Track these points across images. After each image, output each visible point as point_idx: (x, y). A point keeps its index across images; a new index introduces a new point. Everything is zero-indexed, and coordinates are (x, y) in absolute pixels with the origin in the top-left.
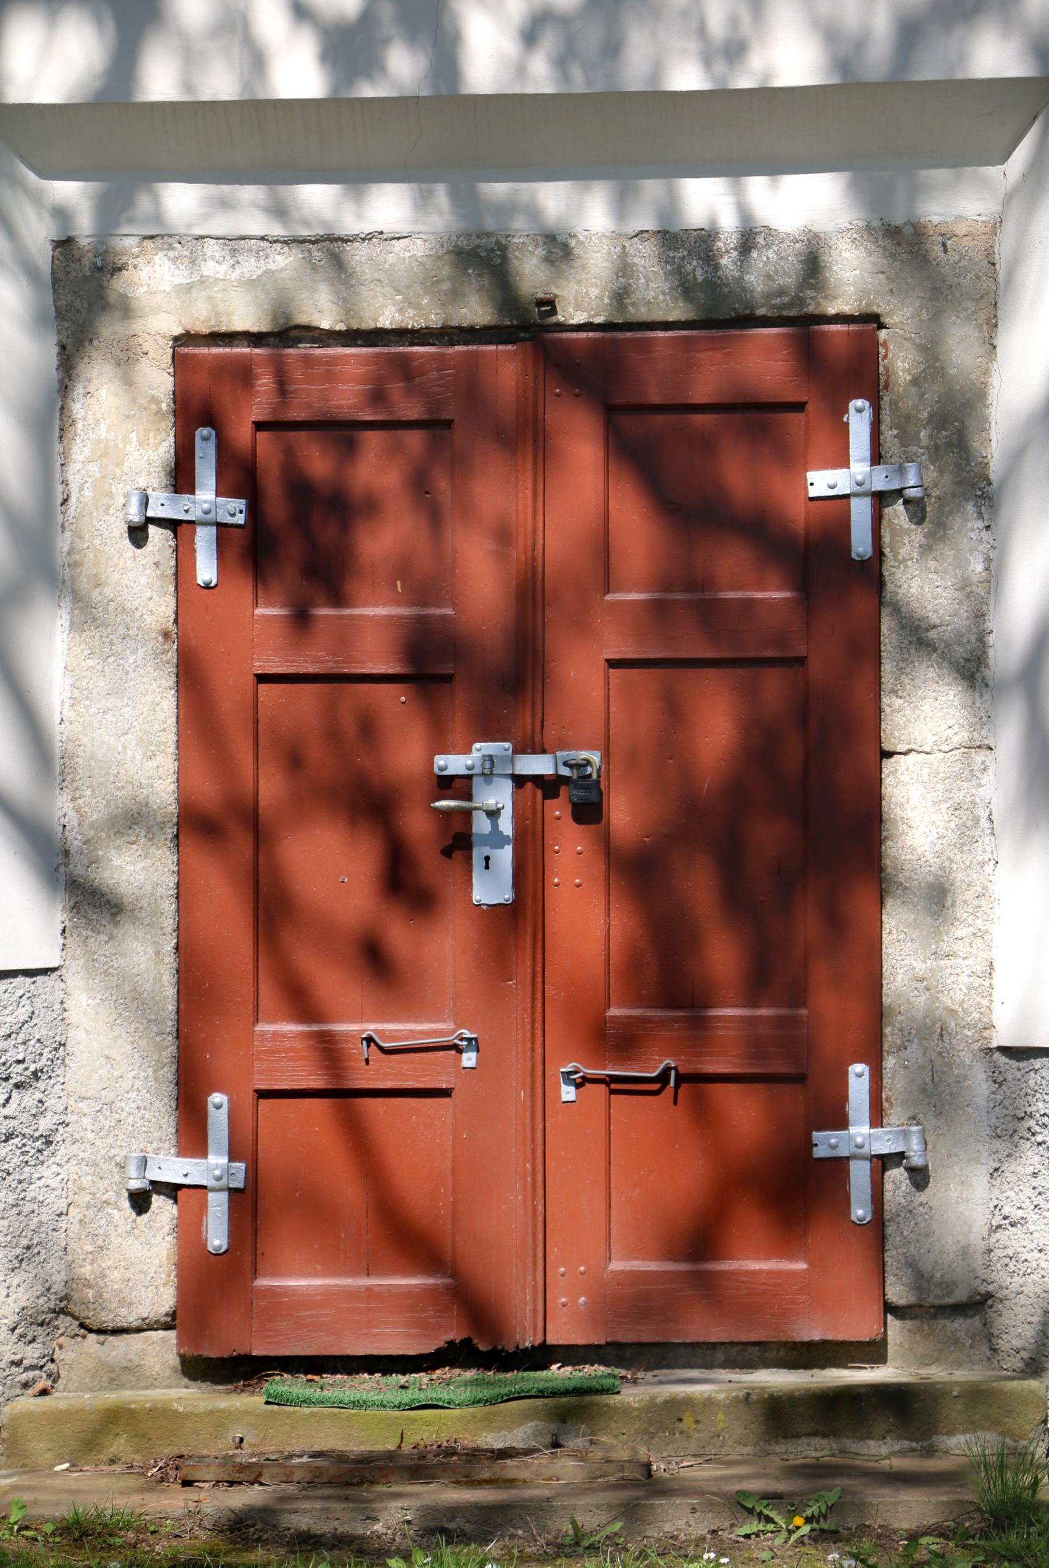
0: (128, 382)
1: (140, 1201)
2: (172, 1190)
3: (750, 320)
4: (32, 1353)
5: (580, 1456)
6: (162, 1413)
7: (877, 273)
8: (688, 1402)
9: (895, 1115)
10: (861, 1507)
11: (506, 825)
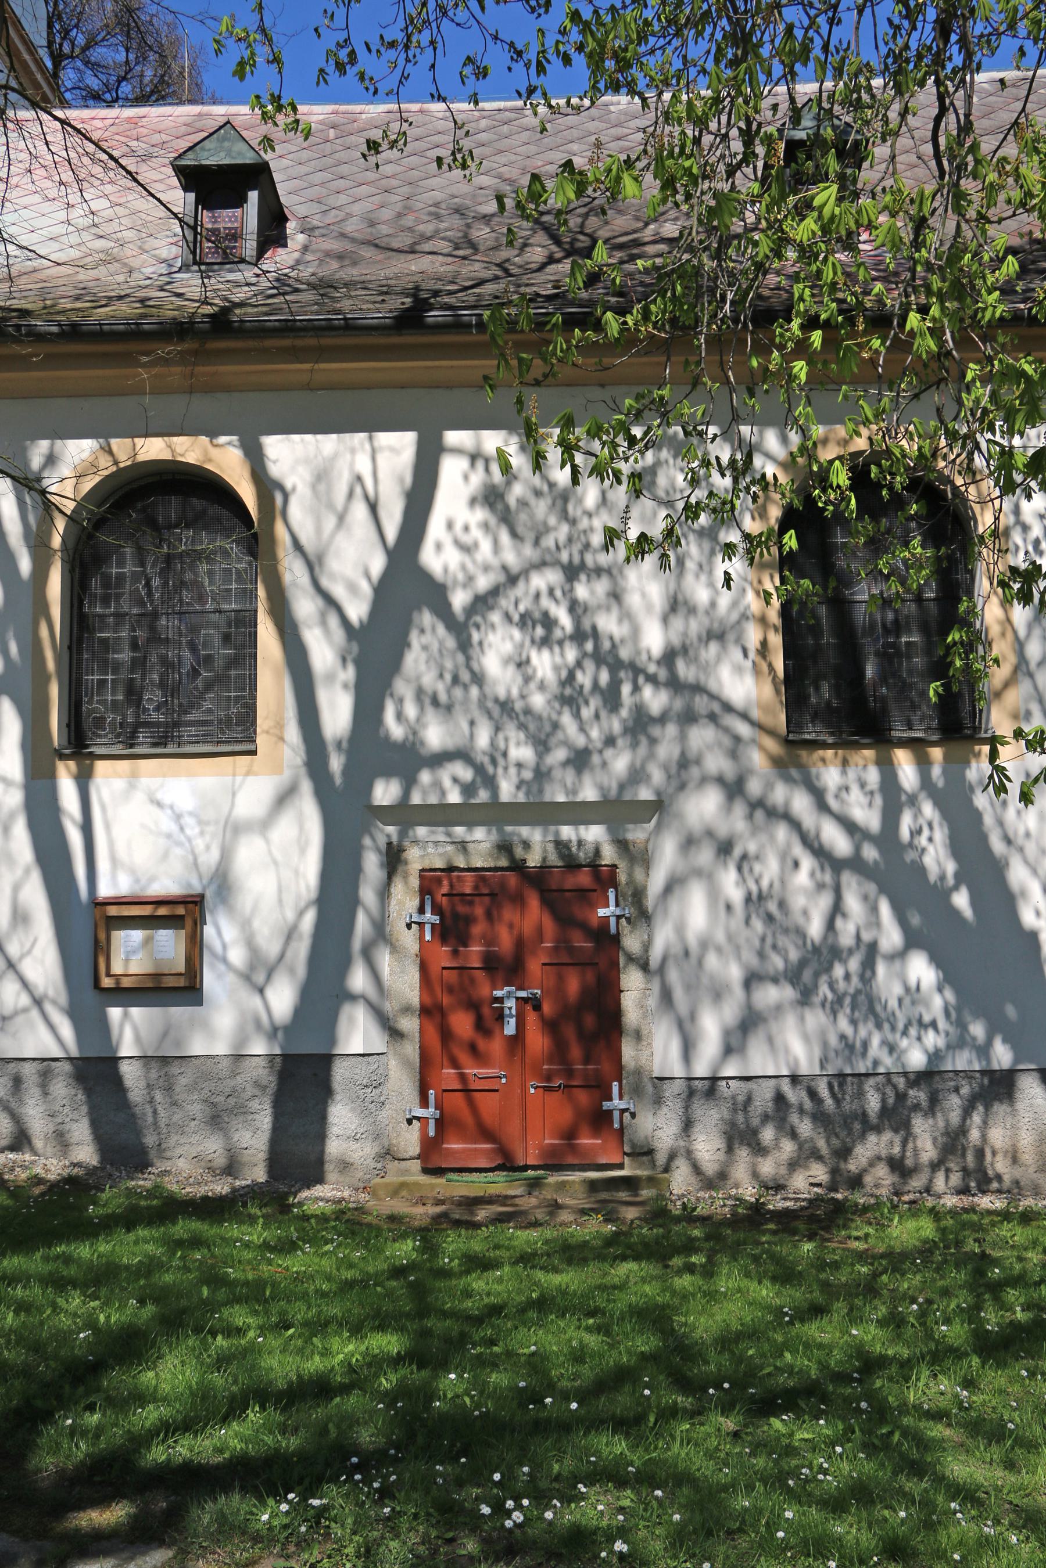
0: (406, 883)
1: (409, 1122)
2: (418, 1119)
3: (581, 866)
4: (379, 1166)
5: (537, 1197)
6: (416, 1184)
7: (46, 1094)
8: (567, 1182)
9: (626, 1097)
10: (618, 1212)
11: (514, 1012)
